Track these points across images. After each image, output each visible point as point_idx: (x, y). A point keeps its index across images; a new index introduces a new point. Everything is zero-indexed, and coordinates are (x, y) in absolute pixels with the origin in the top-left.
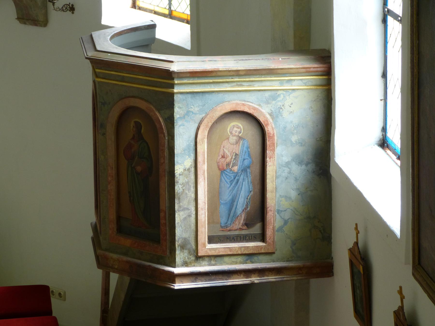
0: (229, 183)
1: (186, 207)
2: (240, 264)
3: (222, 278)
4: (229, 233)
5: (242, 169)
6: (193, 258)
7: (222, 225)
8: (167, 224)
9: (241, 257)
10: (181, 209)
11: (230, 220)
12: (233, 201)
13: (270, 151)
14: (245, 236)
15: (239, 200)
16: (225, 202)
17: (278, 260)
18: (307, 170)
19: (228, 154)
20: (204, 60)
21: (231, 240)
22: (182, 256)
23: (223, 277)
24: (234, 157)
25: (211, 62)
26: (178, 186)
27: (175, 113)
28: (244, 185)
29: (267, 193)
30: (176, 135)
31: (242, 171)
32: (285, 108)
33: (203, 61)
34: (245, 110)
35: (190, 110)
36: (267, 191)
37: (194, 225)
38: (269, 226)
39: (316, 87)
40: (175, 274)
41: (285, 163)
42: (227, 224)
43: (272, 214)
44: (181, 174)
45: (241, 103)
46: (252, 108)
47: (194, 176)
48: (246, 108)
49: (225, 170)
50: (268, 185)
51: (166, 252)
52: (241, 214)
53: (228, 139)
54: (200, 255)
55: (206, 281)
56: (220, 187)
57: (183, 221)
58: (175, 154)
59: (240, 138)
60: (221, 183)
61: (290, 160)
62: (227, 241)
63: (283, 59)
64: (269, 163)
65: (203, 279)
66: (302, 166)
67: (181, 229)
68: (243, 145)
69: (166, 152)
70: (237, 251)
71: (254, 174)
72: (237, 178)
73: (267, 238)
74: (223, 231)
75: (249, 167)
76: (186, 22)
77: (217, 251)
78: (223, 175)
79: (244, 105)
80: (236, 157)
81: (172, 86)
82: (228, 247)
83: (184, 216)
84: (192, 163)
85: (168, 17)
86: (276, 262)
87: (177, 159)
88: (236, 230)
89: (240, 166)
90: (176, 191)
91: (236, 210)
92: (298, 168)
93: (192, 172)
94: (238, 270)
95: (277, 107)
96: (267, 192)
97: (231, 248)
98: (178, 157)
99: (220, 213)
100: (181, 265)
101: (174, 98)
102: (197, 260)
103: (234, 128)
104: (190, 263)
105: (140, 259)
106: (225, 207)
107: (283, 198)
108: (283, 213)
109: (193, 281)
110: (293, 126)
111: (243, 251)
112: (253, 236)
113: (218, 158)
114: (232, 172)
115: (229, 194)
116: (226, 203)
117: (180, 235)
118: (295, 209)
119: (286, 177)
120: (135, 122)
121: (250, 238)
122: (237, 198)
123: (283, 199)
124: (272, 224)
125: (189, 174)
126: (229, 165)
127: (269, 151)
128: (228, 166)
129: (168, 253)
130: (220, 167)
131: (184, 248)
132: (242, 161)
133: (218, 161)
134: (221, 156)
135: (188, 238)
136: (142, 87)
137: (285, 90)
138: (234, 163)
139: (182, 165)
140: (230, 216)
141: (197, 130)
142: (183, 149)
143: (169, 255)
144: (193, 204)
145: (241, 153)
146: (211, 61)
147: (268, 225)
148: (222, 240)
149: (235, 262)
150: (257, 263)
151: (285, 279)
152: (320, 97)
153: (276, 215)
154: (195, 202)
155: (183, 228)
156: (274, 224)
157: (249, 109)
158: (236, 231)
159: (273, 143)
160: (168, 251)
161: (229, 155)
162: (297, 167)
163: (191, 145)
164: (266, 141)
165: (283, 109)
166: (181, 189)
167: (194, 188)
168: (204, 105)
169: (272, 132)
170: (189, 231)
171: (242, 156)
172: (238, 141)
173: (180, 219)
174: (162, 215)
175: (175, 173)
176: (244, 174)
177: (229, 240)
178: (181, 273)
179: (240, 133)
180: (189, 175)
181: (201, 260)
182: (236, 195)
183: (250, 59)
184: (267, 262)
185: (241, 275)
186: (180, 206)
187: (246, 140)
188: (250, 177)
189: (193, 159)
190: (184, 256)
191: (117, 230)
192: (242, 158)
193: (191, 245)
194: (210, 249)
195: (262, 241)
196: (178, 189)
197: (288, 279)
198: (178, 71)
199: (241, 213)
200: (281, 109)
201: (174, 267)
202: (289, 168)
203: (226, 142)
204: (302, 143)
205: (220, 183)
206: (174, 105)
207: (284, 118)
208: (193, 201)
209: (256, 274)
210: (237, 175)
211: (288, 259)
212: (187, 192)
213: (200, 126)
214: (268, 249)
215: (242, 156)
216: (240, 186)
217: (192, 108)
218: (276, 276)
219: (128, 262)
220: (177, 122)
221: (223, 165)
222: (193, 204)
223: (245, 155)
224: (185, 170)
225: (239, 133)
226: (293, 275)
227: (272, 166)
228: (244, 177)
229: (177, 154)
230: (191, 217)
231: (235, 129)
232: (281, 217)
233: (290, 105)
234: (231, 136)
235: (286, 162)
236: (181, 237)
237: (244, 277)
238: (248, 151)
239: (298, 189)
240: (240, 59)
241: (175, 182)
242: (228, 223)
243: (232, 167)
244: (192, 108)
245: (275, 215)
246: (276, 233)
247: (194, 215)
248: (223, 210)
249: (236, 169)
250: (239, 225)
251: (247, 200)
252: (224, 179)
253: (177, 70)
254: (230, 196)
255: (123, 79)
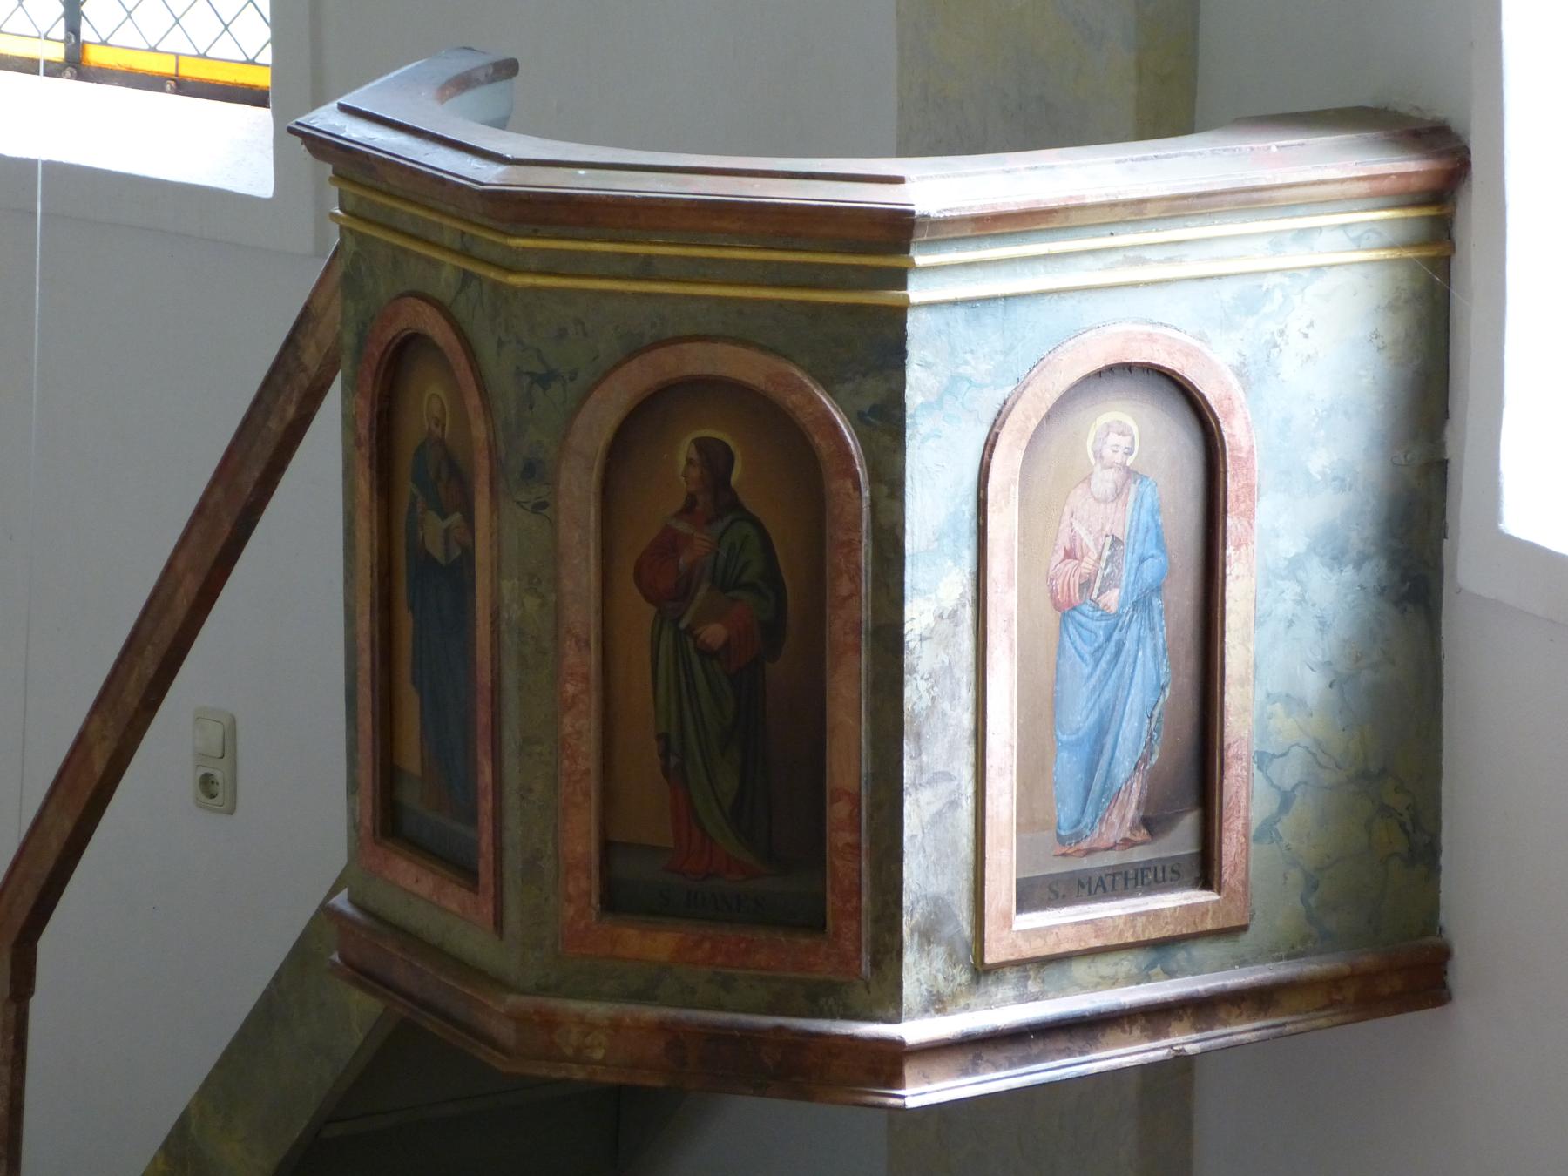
0: (1088, 662)
1: (940, 768)
2: (1127, 986)
3: (1069, 1049)
4: (1085, 863)
5: (1135, 598)
6: (963, 977)
7: (1063, 833)
8: (864, 846)
9: (1130, 957)
10: (925, 778)
11: (1089, 809)
12: (1102, 730)
13: (1238, 518)
14: (1142, 870)
15: (1124, 724)
16: (1074, 737)
17: (1260, 957)
18: (1361, 586)
19: (1088, 540)
20: (924, 175)
21: (1093, 892)
22: (924, 972)
23: (1070, 1045)
24: (1107, 553)
25: (1037, 172)
26: (917, 686)
27: (911, 386)
28: (1139, 663)
29: (1226, 689)
30: (912, 478)
31: (1135, 605)
32: (1287, 344)
33: (1008, 172)
34: (1155, 359)
35: (961, 370)
36: (1228, 681)
37: (969, 841)
38: (1231, 820)
39: (1383, 254)
40: (910, 1046)
41: (1286, 563)
42: (1078, 828)
43: (1241, 770)
44: (926, 634)
45: (1142, 333)
46: (1180, 350)
47: (973, 638)
48: (1158, 350)
49: (1074, 608)
50: (1230, 655)
51: (857, 962)
52: (1129, 783)
53: (1087, 479)
54: (992, 962)
55: (1012, 1065)
56: (1057, 679)
57: (929, 826)
58: (907, 554)
59: (1130, 473)
60: (1061, 662)
61: (1302, 548)
62: (1078, 896)
63: (1283, 147)
64: (1235, 564)
65: (1000, 1057)
66: (1342, 571)
67: (922, 862)
68: (1138, 504)
69: (863, 549)
70: (1121, 934)
71: (1176, 616)
72: (1116, 636)
73: (1224, 869)
74: (1064, 855)
75: (1157, 589)
76: (172, 87)
77: (1051, 939)
78: (1067, 629)
79: (1150, 337)
80: (1115, 550)
81: (899, 279)
82: (1091, 920)
83: (934, 809)
84: (964, 587)
85: (68, 74)
86: (1252, 965)
87: (914, 575)
88: (1111, 848)
89: (1127, 585)
90: (907, 706)
91: (1112, 766)
92: (1330, 579)
93: (965, 624)
94: (1127, 1007)
95: (1260, 340)
96: (1226, 683)
97: (1101, 924)
98: (915, 568)
99: (1055, 784)
100: (919, 1011)
101: (908, 325)
102: (978, 983)
103: (1108, 434)
104: (954, 996)
105: (721, 1008)
106: (1075, 759)
107: (1278, 704)
108: (1277, 762)
109: (967, 1069)
110: (1314, 413)
111: (1141, 929)
112: (1168, 870)
113: (1050, 561)
114: (1099, 613)
115: (1087, 702)
116: (1079, 742)
117: (918, 888)
118: (1318, 743)
119: (1290, 617)
120: (702, 445)
121: (1160, 875)
122: (1117, 716)
123: (1278, 708)
124: (1242, 813)
125: (954, 635)
126: (1088, 588)
127: (1235, 518)
128: (1087, 591)
129: (865, 968)
130: (1059, 597)
131: (932, 939)
132: (1135, 565)
133: (1051, 573)
134: (1062, 553)
135: (946, 897)
136: (749, 293)
137: (1289, 272)
138: (1108, 575)
139: (929, 599)
140: (1091, 792)
141: (986, 453)
142: (934, 534)
143: (869, 976)
144: (966, 753)
145: (1132, 534)
146: (1036, 168)
147: (1229, 818)
148: (1061, 894)
149: (1112, 979)
150: (1186, 975)
151: (1288, 1028)
152: (1404, 290)
153: (1253, 774)
154: (973, 745)
155: (931, 856)
156: (1247, 809)
157: (1169, 354)
158: (1110, 852)
159: (1248, 485)
160: (866, 958)
161: (1091, 545)
162: (1324, 576)
163: (964, 512)
164: (1225, 477)
165: (1281, 347)
166: (926, 696)
167: (972, 687)
168: (1012, 348)
169: (1244, 443)
170: (950, 867)
171: (1136, 547)
172: (1124, 485)
173: (921, 821)
174: (837, 811)
175: (906, 632)
176: (1139, 619)
177: (1086, 890)
178: (927, 1043)
179: (1129, 452)
180: (953, 636)
181: (990, 981)
182: (1111, 707)
183: (1172, 153)
184: (1222, 968)
185: (1134, 1028)
186: (921, 767)
187: (1151, 479)
188: (1162, 630)
189: (968, 570)
190: (934, 972)
191: (602, 900)
192: (1135, 555)
193: (958, 924)
194: (1028, 934)
195: (1201, 883)
196: (915, 699)
197: (1301, 1026)
198: (942, 216)
199: (1128, 776)
200: (1276, 346)
201: (896, 1019)
202: (1300, 582)
203: (1079, 491)
204: (1343, 480)
205: (1058, 661)
206: (902, 354)
207: (1283, 381)
208: (966, 741)
209: (1185, 1018)
210: (1117, 624)
211: (1292, 951)
212: (946, 706)
213: (1000, 436)
214: (1228, 914)
215: (1134, 545)
216: (1128, 670)
217: (966, 363)
218: (1255, 1020)
219: (662, 1027)
220: (915, 424)
221: (1069, 589)
222: (967, 753)
223: (1145, 540)
224: (941, 616)
225: (1126, 454)
226: (1312, 1011)
227: (1243, 576)
228: (1140, 629)
229: (913, 555)
230: (960, 809)
231: (1114, 439)
232: (1269, 779)
233: (1306, 331)
234: (1098, 468)
235: (1291, 561)
236: (923, 893)
237: (1145, 1036)
238: (1157, 526)
239: (1330, 663)
240: (1135, 156)
241: (905, 670)
242: (1084, 823)
243: (1098, 596)
244: (966, 363)
245: (1251, 775)
246: (1253, 846)
247: (969, 800)
248: (1066, 768)
249: (1112, 599)
250: (1120, 827)
251: (1150, 723)
252: (1072, 643)
253: (939, 212)
254: (1091, 710)
255: (646, 269)
